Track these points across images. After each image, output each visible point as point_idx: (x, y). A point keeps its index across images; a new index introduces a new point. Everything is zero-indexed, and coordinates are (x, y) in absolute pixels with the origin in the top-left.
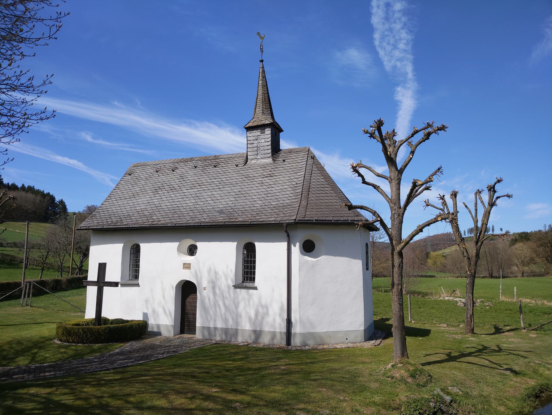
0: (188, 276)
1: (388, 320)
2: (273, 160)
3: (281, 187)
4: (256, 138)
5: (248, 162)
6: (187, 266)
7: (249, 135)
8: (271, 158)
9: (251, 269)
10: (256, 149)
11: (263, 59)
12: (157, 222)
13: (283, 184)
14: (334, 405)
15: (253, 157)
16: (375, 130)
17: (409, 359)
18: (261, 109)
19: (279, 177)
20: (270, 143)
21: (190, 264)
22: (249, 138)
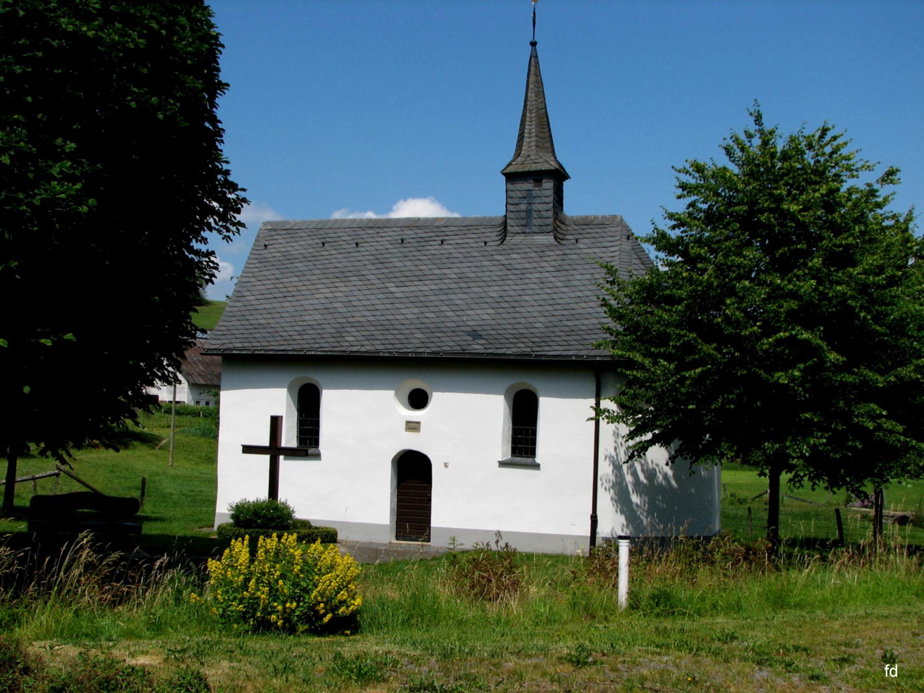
0: (413, 443)
1: (216, 277)
2: (556, 238)
3: (579, 294)
4: (525, 194)
5: (507, 238)
6: (413, 426)
7: (511, 187)
8: (552, 234)
9: (527, 434)
10: (523, 215)
11: (536, 39)
12: (359, 347)
13: (581, 288)
14: (683, 664)
15: (518, 229)
16: (748, 179)
17: (141, 478)
18: (534, 139)
19: (572, 272)
20: (551, 205)
21: (419, 423)
22: (510, 194)
